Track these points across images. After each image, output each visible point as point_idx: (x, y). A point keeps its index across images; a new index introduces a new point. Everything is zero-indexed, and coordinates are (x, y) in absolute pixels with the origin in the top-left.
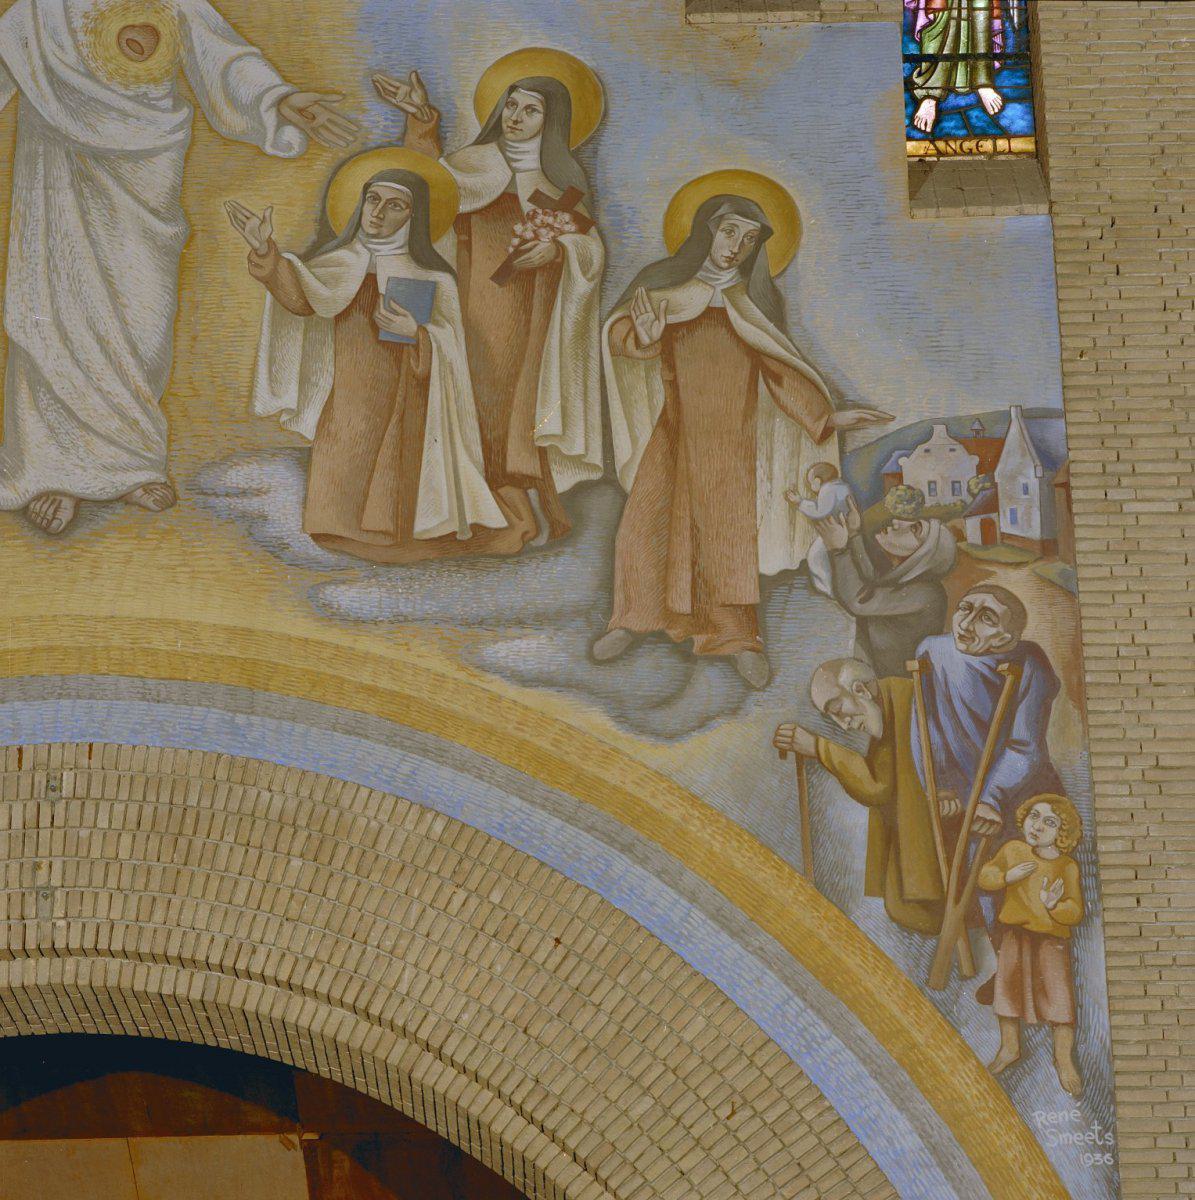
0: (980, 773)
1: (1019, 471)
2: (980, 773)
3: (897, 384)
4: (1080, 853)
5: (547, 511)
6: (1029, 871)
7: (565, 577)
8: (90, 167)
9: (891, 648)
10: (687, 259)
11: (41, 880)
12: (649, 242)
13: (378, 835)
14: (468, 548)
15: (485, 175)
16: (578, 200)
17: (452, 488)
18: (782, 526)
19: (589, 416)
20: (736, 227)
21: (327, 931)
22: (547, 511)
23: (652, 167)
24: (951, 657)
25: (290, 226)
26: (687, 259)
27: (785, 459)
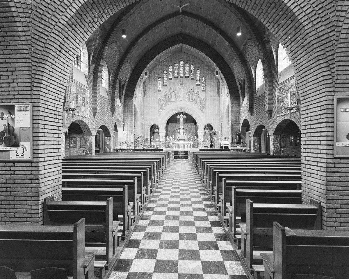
0: (230, 110)
1: (204, 99)
2: (230, 110)
3: (201, 97)
4: (205, 109)
5: (193, 100)
6: (204, 109)
7: (193, 102)
8: (181, 91)
9: (201, 104)
10: (196, 93)
11: (302, 99)
12: (195, 93)
13: (318, 65)
14: (191, 101)
15: (191, 91)
16: (194, 92)
17: (191, 100)
18: (198, 100)
19: (194, 97)
20: (198, 92)
21: (311, 6)
22: (193, 100)
23: (195, 91)
24: (202, 104)
25: (186, 92)
26: (196, 93)
27: (199, 99)
